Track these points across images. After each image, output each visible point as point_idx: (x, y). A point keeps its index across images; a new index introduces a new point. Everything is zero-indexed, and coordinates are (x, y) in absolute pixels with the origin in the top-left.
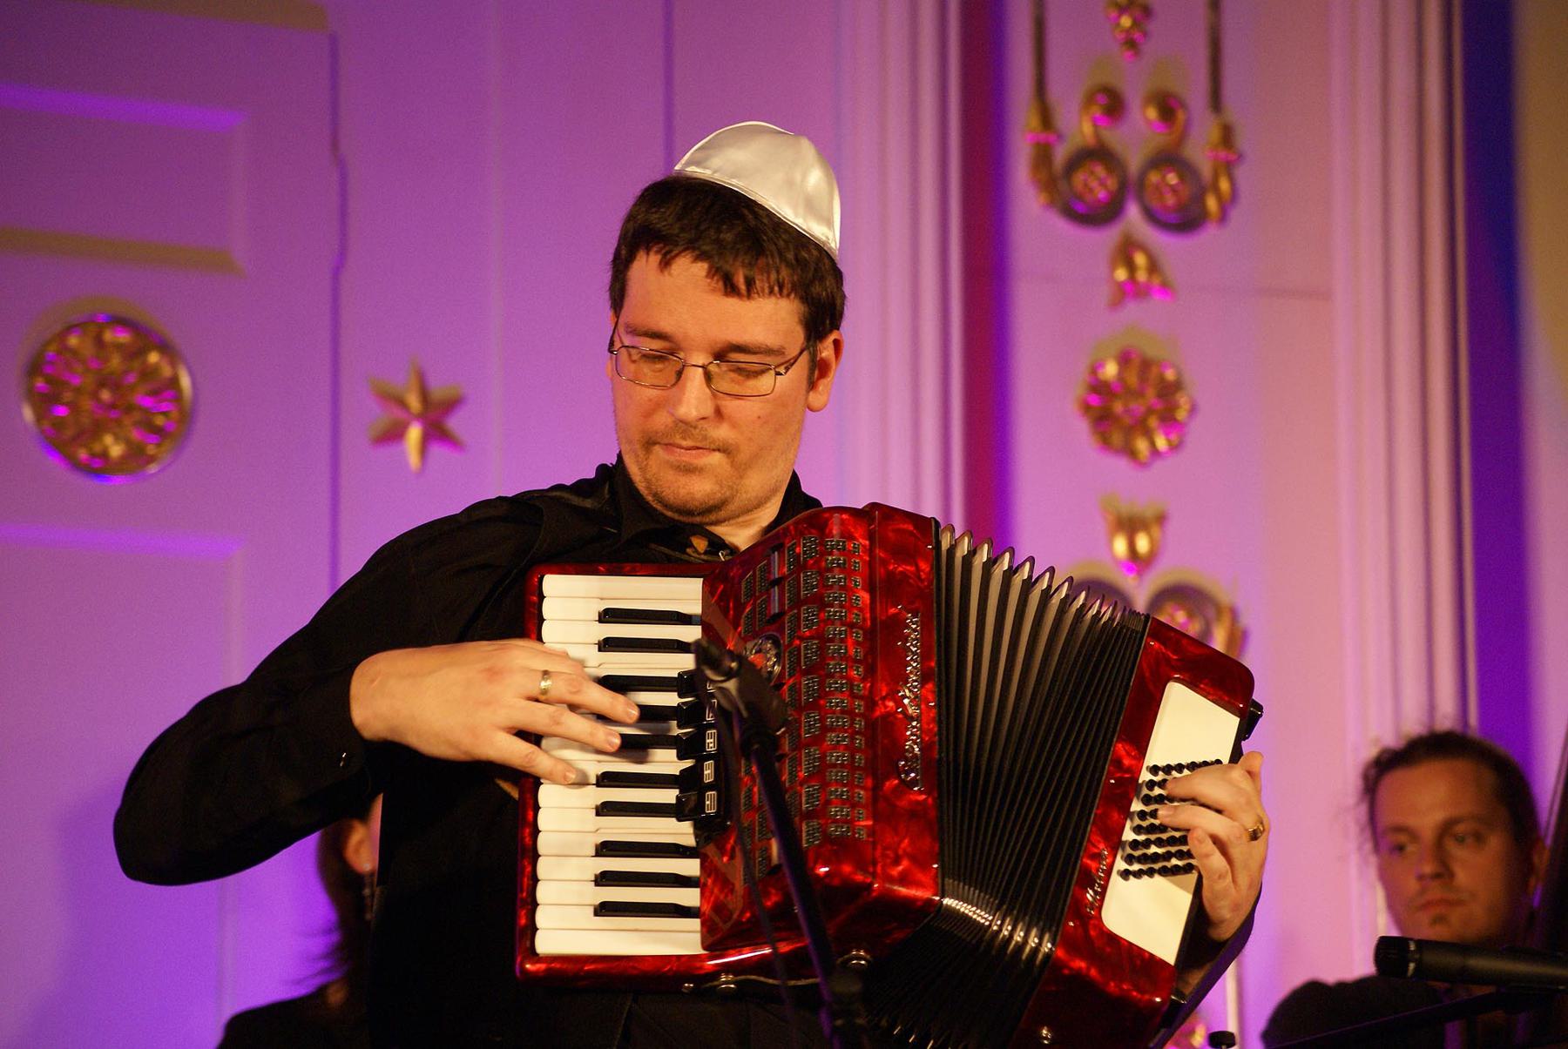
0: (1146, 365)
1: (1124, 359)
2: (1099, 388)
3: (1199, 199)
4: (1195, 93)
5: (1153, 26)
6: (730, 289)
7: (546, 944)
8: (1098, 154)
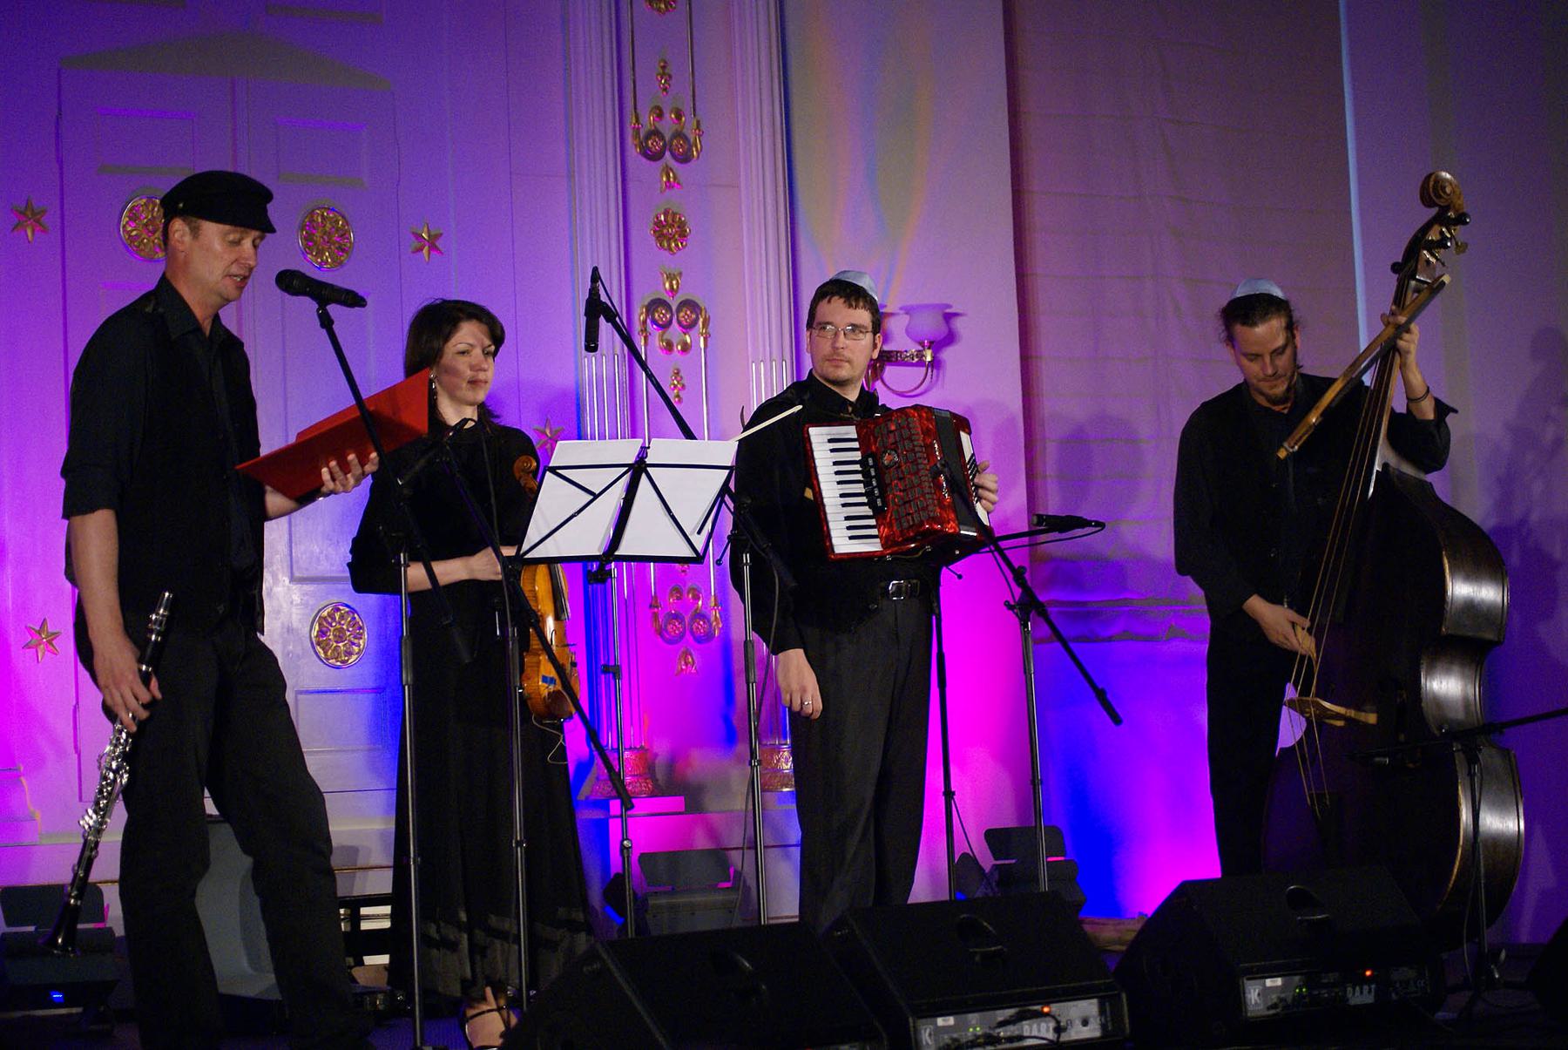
0: (674, 214)
1: (666, 213)
2: (658, 224)
3: (690, 150)
4: (687, 108)
5: (673, 82)
6: (850, 306)
7: (838, 550)
8: (655, 133)
